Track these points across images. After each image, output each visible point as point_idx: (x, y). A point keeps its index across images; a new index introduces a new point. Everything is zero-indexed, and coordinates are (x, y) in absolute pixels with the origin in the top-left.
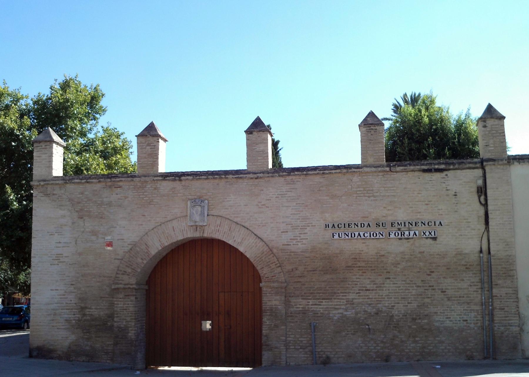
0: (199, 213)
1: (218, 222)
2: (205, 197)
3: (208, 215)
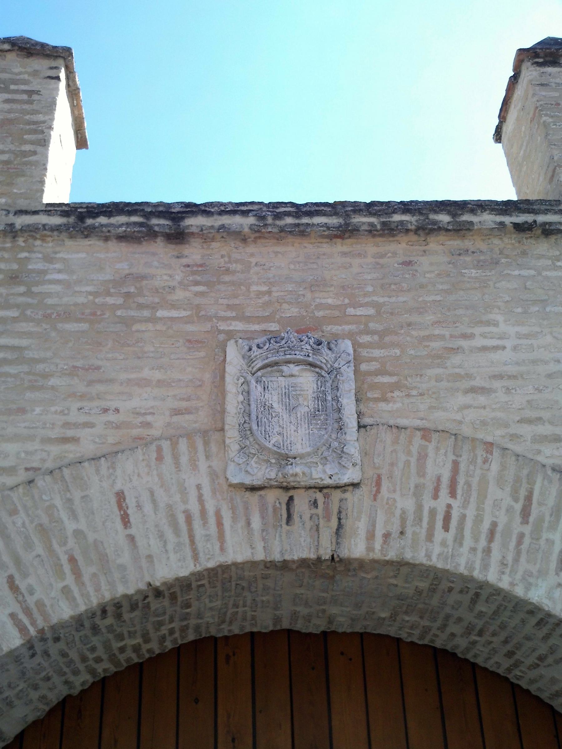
0: (307, 404)
1: (439, 465)
2: (336, 329)
3: (361, 426)
